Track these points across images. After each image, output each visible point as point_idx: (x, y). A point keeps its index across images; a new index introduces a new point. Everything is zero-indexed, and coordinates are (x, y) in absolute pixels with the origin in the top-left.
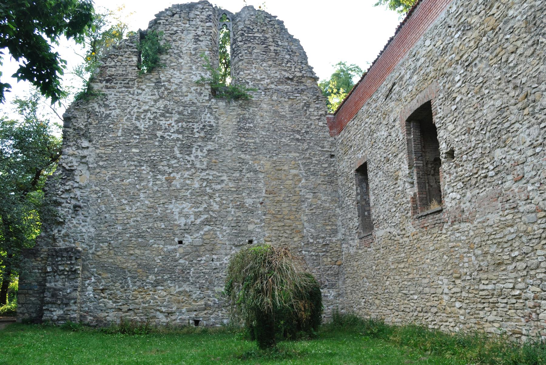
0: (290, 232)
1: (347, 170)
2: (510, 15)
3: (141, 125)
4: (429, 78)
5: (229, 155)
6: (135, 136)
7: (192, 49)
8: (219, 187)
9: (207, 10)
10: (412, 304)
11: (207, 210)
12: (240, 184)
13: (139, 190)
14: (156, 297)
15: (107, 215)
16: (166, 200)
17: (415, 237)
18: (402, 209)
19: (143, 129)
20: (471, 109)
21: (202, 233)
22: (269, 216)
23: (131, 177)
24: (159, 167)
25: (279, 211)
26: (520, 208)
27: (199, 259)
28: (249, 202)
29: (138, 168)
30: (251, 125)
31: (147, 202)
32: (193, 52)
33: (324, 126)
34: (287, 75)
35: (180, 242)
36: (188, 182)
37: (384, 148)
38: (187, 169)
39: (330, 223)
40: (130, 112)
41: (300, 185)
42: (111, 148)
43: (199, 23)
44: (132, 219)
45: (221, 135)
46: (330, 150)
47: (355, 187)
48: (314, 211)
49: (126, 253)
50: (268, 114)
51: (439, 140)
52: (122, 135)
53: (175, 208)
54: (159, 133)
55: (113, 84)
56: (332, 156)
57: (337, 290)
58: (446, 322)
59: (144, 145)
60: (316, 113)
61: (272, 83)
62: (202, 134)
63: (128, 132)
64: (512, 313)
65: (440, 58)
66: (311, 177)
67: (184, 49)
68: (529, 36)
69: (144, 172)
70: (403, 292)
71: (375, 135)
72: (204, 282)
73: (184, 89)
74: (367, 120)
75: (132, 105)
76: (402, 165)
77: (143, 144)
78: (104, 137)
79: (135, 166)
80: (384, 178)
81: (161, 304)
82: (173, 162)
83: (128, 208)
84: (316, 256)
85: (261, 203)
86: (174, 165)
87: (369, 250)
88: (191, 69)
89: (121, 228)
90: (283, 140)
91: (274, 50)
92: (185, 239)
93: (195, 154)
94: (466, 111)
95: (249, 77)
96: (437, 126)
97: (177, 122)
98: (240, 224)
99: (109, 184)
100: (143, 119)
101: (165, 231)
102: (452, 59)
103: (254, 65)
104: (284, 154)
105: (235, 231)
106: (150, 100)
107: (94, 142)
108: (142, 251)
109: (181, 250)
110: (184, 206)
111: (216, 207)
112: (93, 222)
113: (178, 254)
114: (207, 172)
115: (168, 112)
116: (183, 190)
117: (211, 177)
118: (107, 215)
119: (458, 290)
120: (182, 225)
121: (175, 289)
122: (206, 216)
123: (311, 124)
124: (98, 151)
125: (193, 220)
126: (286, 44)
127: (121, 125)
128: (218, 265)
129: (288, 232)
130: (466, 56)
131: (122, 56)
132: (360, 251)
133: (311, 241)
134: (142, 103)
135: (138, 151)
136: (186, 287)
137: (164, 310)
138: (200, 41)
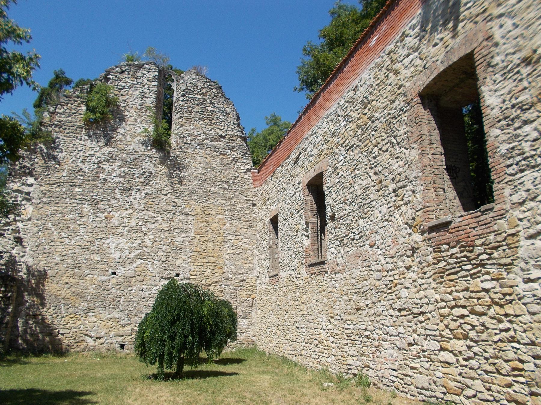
0: (213, 268)
1: (264, 218)
2: (376, 117)
3: (86, 168)
4: (323, 154)
5: (165, 199)
6: (79, 177)
7: (137, 104)
8: (153, 226)
9: (153, 70)
10: (302, 336)
11: (141, 246)
12: (172, 224)
13: (79, 225)
14: (87, 322)
15: (46, 247)
16: (103, 235)
17: (306, 281)
18: (299, 256)
19: (87, 171)
20: (348, 184)
21: (135, 265)
22: (195, 254)
23: (72, 213)
24: (99, 206)
25: (204, 250)
26: (372, 267)
27: (130, 289)
28: (178, 239)
29: (80, 206)
30: (186, 174)
31: (86, 237)
32: (139, 107)
33: (248, 179)
34: (221, 133)
35: (114, 273)
36: (126, 220)
37: (291, 204)
38: (126, 209)
39: (248, 262)
40: (75, 156)
41: (225, 228)
42: (55, 186)
43: (146, 81)
44: (70, 251)
45: (158, 181)
46: (252, 199)
47: (268, 233)
48: (235, 251)
49: (61, 282)
50: (201, 165)
51: (326, 204)
52: (67, 176)
53: (111, 243)
54: (102, 176)
55: (61, 129)
56: (254, 205)
57: (250, 320)
58: (323, 353)
59: (87, 186)
60: (242, 167)
61: (207, 139)
62: (142, 180)
63: (74, 173)
64: (365, 350)
65: (331, 140)
66: (235, 221)
67: (131, 103)
68: (386, 136)
69: (85, 209)
70: (296, 325)
71: (285, 192)
72: (132, 309)
73: (128, 138)
74: (281, 179)
75: (79, 149)
76: (302, 220)
77: (86, 184)
78: (50, 176)
79: (78, 204)
80: (289, 229)
81: (90, 329)
82: (113, 202)
83: (67, 241)
84: (234, 289)
85: (190, 242)
86: (115, 205)
87: (275, 287)
88: (136, 121)
89: (59, 259)
90: (213, 189)
91: (211, 111)
92: (118, 271)
93: (134, 197)
94: (344, 184)
95: (187, 132)
96: (326, 193)
97: (120, 167)
98: (169, 259)
99: (51, 219)
100: (88, 162)
101: (100, 263)
102: (339, 141)
103: (192, 123)
104: (213, 201)
105: (165, 265)
106: (96, 146)
107: (39, 180)
108: (77, 281)
109: (114, 281)
110: (121, 241)
111: (149, 243)
112: (32, 253)
113: (111, 284)
114: (144, 212)
115: (111, 158)
116: (121, 227)
117: (146, 217)
118: (46, 247)
119: (332, 327)
120: (117, 257)
121: (105, 315)
122: (139, 251)
123: (238, 176)
124: (42, 188)
125: (127, 254)
126: (222, 106)
127: (66, 166)
128: (147, 294)
129: (210, 267)
130: (347, 142)
131: (72, 104)
132: (269, 288)
133: (231, 276)
134: (87, 148)
135: (81, 190)
136: (116, 314)
137: (93, 335)
138: (146, 97)
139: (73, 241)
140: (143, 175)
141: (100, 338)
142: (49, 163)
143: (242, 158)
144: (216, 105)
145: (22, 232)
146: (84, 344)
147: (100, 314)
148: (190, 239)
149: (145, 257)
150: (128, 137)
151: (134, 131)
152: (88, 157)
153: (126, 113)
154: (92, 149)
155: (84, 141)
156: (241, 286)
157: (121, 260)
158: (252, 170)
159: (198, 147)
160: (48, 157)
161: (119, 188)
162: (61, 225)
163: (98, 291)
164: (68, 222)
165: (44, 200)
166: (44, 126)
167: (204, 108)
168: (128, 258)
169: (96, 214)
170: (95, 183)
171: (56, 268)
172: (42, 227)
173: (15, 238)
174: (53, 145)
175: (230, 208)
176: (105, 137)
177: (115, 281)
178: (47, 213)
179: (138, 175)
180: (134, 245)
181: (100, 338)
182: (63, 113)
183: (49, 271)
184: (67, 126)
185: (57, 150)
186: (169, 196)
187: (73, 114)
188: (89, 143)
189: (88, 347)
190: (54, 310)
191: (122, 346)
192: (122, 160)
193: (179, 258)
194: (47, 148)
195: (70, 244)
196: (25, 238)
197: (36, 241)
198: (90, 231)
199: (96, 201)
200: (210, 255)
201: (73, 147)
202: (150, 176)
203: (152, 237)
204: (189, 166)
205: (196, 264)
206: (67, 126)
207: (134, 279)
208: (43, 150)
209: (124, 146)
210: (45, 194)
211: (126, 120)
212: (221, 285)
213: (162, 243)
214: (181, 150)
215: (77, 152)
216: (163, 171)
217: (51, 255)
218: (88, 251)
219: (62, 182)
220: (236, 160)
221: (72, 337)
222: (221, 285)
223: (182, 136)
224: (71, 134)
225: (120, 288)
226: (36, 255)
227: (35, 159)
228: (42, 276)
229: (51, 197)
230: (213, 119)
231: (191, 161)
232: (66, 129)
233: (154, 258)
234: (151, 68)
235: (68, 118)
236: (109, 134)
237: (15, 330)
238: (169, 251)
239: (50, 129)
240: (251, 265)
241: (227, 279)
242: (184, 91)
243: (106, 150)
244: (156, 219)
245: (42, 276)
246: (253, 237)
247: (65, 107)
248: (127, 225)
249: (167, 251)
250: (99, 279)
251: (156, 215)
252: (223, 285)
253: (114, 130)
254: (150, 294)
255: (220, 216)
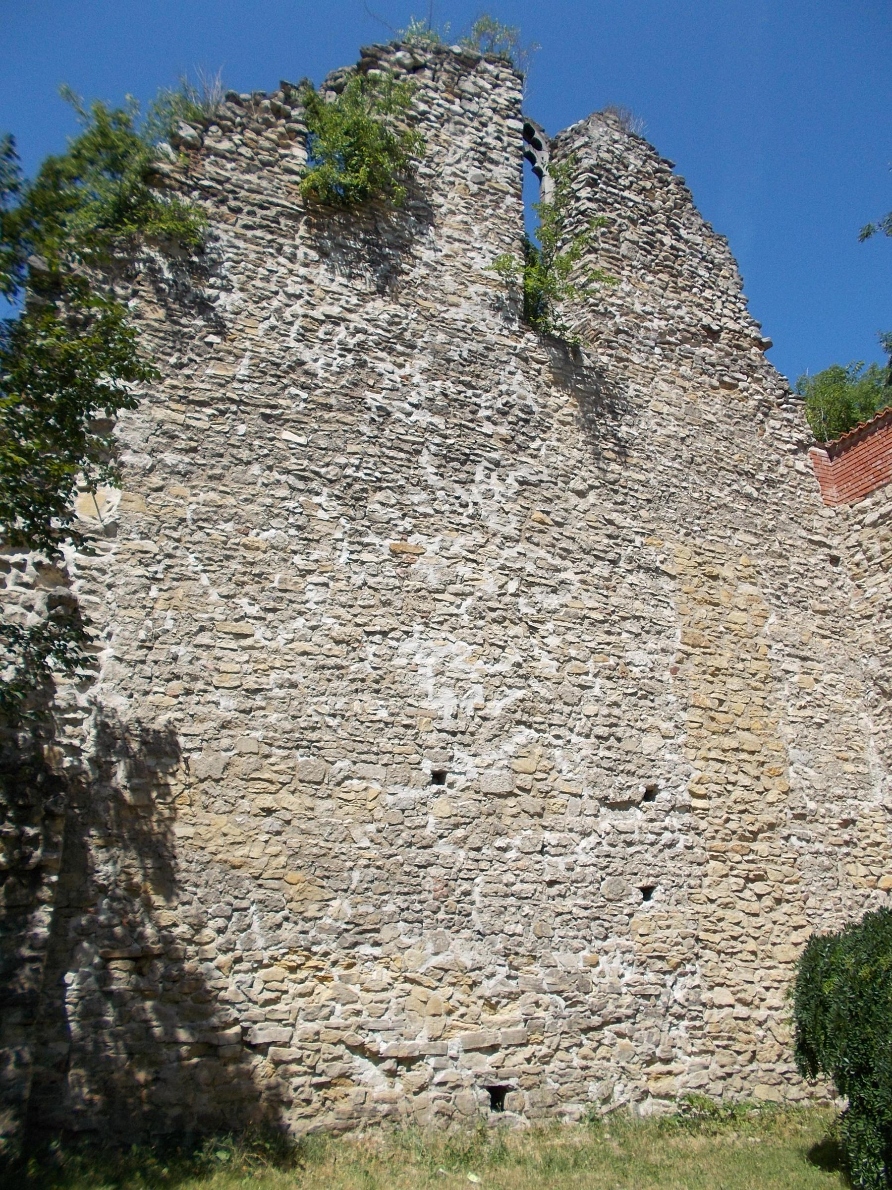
0: (755, 773)
3: (316, 358)
5: (581, 508)
6: (293, 390)
8: (553, 602)
9: (509, 84)
11: (523, 673)
13: (304, 573)
14: (356, 989)
15: (181, 650)
16: (393, 622)
19: (321, 373)
21: (509, 748)
23: (274, 522)
24: (370, 507)
27: (500, 842)
30: (634, 431)
32: (475, 188)
35: (438, 777)
38: (460, 529)
39: (852, 755)
40: (278, 311)
42: (209, 411)
43: (489, 113)
44: (273, 675)
49: (245, 804)
50: (673, 410)
52: (250, 379)
54: (373, 399)
55: (224, 209)
59: (325, 426)
60: (785, 434)
62: (504, 430)
66: (792, 610)
67: (449, 170)
77: (321, 420)
78: (187, 371)
79: (292, 488)
81: (372, 1023)
82: (416, 499)
83: (260, 632)
84: (830, 854)
86: (421, 509)
88: (469, 231)
89: (233, 704)
91: (672, 247)
93: (484, 487)
97: (431, 375)
100: (324, 341)
101: (390, 732)
104: (721, 533)
106: (345, 291)
108: (308, 802)
109: (442, 807)
110: (453, 649)
111: (546, 665)
112: (123, 671)
114: (520, 547)
116: (446, 596)
117: (530, 568)
118: (181, 650)
120: (447, 713)
121: (421, 956)
122: (520, 694)
125: (479, 701)
126: (699, 240)
128: (562, 867)
129: (747, 767)
133: (812, 805)
136: (462, 952)
137: (383, 1048)
139: (283, 636)
140: (505, 414)
141: (409, 1061)
142: (184, 321)
143: (779, 405)
144: (682, 232)
145: (80, 582)
146: (353, 1090)
147: (402, 949)
148: (672, 659)
149: (539, 719)
150: (447, 278)
151: (467, 261)
152: (323, 322)
153: (437, 199)
154: (336, 297)
155: (306, 265)
156: (847, 843)
157: (461, 725)
158: (812, 449)
159: (657, 350)
160: (178, 299)
161: (433, 448)
162: (234, 565)
163: (387, 850)
164: (260, 556)
165: (170, 458)
166: (163, 187)
167: (652, 233)
168: (484, 719)
169: (361, 534)
170: (349, 419)
171: (225, 742)
172: (160, 568)
173: (52, 601)
174: (195, 259)
175: (770, 561)
176: (373, 263)
177: (446, 811)
178: (179, 513)
179: (489, 413)
180: (498, 667)
181: (409, 1061)
182: (231, 156)
183: (195, 756)
184: (246, 201)
185: (212, 280)
186: (592, 497)
187: (265, 164)
188: (320, 275)
189: (369, 1105)
190: (220, 931)
191: (497, 1095)
192: (435, 353)
193: (652, 728)
194: (171, 266)
195: (273, 645)
196: (95, 606)
197: (139, 624)
198: (343, 599)
199: (357, 487)
200: (739, 722)
201: (266, 279)
202: (527, 421)
203: (553, 641)
204: (640, 406)
205: (703, 753)
206: (246, 201)
207: (511, 802)
208: (160, 270)
209: (439, 306)
210: (173, 437)
211: (437, 221)
212: (787, 838)
213: (590, 666)
214: (610, 352)
215: (281, 297)
216: (565, 411)
217: (200, 685)
218: (340, 678)
219: (233, 401)
220: (765, 407)
221: (299, 1061)
222: (787, 838)
223: (601, 308)
224: (259, 233)
225: (466, 837)
226: (139, 683)
227: (127, 299)
228: (162, 748)
229: (194, 450)
230: (680, 274)
231: (644, 390)
232: (238, 211)
233: (571, 723)
234: (502, 76)
235: (247, 177)
236: (386, 257)
237: (51, 1032)
238: (614, 698)
239: (186, 201)
240: (861, 768)
241: (802, 817)
242: (591, 171)
243: (379, 307)
244: (562, 576)
245: (162, 748)
246: (851, 669)
247: (237, 138)
248: (468, 589)
249: (608, 701)
250: (390, 800)
251: (557, 562)
252: (793, 839)
253: (404, 246)
254: (570, 869)
255: (746, 588)
